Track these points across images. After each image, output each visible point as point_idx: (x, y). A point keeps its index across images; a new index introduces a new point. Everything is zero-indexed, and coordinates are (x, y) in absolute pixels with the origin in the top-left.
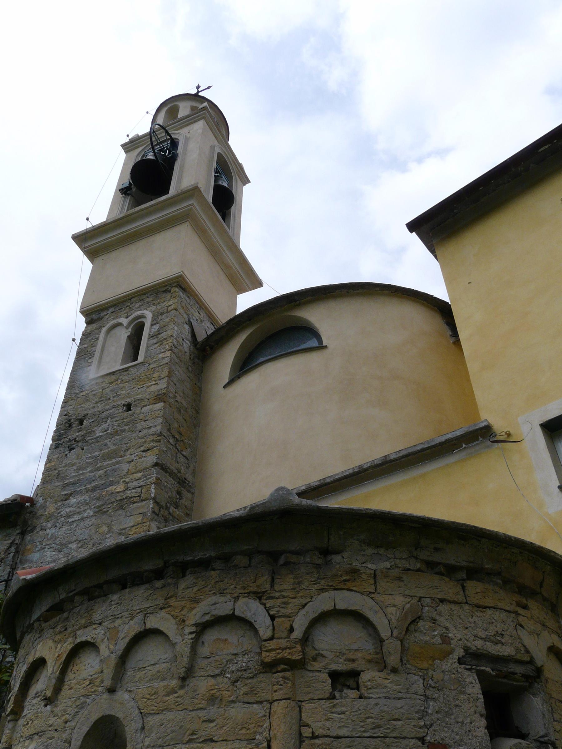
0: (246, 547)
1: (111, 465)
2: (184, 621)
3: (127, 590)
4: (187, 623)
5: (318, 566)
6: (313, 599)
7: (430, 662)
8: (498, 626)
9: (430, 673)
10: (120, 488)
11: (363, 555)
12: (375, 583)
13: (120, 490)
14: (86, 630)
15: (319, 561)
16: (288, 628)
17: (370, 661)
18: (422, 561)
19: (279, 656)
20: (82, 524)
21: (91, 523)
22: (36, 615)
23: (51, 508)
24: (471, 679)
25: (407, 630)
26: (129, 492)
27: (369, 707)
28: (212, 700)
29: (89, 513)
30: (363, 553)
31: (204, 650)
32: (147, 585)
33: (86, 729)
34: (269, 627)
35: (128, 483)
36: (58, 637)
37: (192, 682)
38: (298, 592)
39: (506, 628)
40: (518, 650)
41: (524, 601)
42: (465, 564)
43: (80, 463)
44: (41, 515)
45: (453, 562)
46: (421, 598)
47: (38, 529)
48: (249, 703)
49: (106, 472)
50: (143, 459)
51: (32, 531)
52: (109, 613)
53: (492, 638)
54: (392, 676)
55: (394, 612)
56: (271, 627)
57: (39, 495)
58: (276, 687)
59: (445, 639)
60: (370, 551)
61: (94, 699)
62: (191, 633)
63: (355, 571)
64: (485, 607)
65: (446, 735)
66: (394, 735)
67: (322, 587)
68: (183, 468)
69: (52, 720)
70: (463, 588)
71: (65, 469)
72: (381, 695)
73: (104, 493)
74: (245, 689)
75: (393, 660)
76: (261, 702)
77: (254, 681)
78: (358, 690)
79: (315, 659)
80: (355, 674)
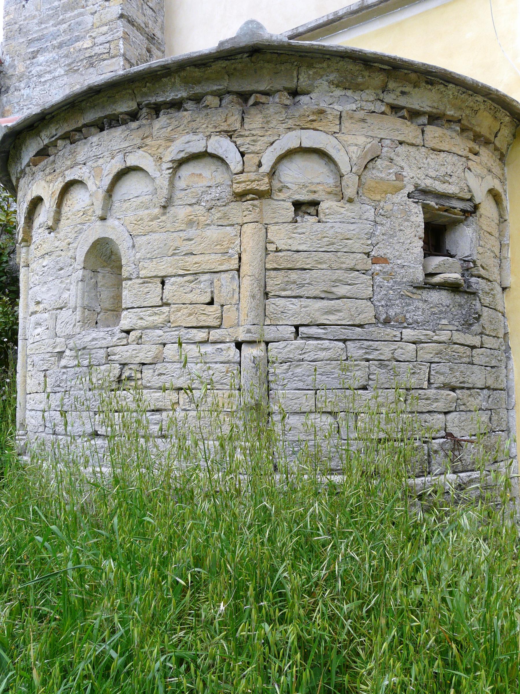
0: (215, 88)
1: (74, 17)
2: (161, 158)
3: (105, 132)
4: (164, 160)
5: (286, 106)
6: (281, 137)
7: (383, 195)
8: (449, 168)
9: (382, 204)
10: (87, 43)
11: (331, 96)
12: (340, 124)
13: (88, 46)
14: (73, 170)
15: (288, 102)
16: (257, 163)
17: (330, 193)
18: (387, 104)
19: (248, 187)
20: (55, 83)
21: (63, 82)
22: (26, 159)
23: (20, 68)
24: (416, 210)
25: (366, 167)
26: (97, 48)
27: (326, 229)
28: (190, 223)
29: (60, 72)
30: (331, 94)
31: (181, 184)
32: (123, 127)
33: (86, 249)
34: (239, 162)
35: (94, 38)
36: (49, 178)
37: (172, 210)
38: (267, 131)
39: (455, 170)
40: (462, 189)
41: (477, 148)
42: (429, 109)
43: (40, 15)
44: (12, 75)
45: (417, 107)
46: (381, 139)
47: (12, 89)
48: (222, 226)
49: (69, 26)
50: (107, 9)
51: (6, 91)
52: (91, 154)
53: (441, 178)
54: (348, 205)
55: (355, 151)
56: (242, 162)
57: (5, 53)
58: (245, 213)
59: (399, 177)
60: (338, 92)
61: (89, 226)
62: (169, 169)
63: (322, 112)
64: (440, 151)
65: (388, 251)
66: (345, 250)
67: (290, 126)
68: (150, 22)
69: (57, 244)
70: (423, 132)
71: (26, 22)
72: (337, 220)
73: (72, 50)
74: (219, 215)
75: (350, 192)
76: (233, 225)
77: (227, 208)
78: (317, 215)
79: (280, 191)
80: (315, 204)
